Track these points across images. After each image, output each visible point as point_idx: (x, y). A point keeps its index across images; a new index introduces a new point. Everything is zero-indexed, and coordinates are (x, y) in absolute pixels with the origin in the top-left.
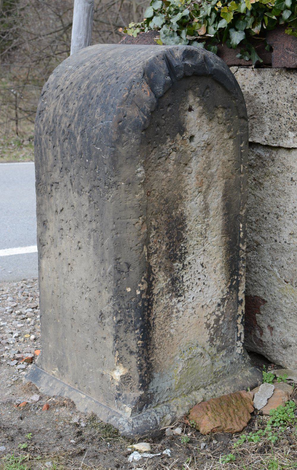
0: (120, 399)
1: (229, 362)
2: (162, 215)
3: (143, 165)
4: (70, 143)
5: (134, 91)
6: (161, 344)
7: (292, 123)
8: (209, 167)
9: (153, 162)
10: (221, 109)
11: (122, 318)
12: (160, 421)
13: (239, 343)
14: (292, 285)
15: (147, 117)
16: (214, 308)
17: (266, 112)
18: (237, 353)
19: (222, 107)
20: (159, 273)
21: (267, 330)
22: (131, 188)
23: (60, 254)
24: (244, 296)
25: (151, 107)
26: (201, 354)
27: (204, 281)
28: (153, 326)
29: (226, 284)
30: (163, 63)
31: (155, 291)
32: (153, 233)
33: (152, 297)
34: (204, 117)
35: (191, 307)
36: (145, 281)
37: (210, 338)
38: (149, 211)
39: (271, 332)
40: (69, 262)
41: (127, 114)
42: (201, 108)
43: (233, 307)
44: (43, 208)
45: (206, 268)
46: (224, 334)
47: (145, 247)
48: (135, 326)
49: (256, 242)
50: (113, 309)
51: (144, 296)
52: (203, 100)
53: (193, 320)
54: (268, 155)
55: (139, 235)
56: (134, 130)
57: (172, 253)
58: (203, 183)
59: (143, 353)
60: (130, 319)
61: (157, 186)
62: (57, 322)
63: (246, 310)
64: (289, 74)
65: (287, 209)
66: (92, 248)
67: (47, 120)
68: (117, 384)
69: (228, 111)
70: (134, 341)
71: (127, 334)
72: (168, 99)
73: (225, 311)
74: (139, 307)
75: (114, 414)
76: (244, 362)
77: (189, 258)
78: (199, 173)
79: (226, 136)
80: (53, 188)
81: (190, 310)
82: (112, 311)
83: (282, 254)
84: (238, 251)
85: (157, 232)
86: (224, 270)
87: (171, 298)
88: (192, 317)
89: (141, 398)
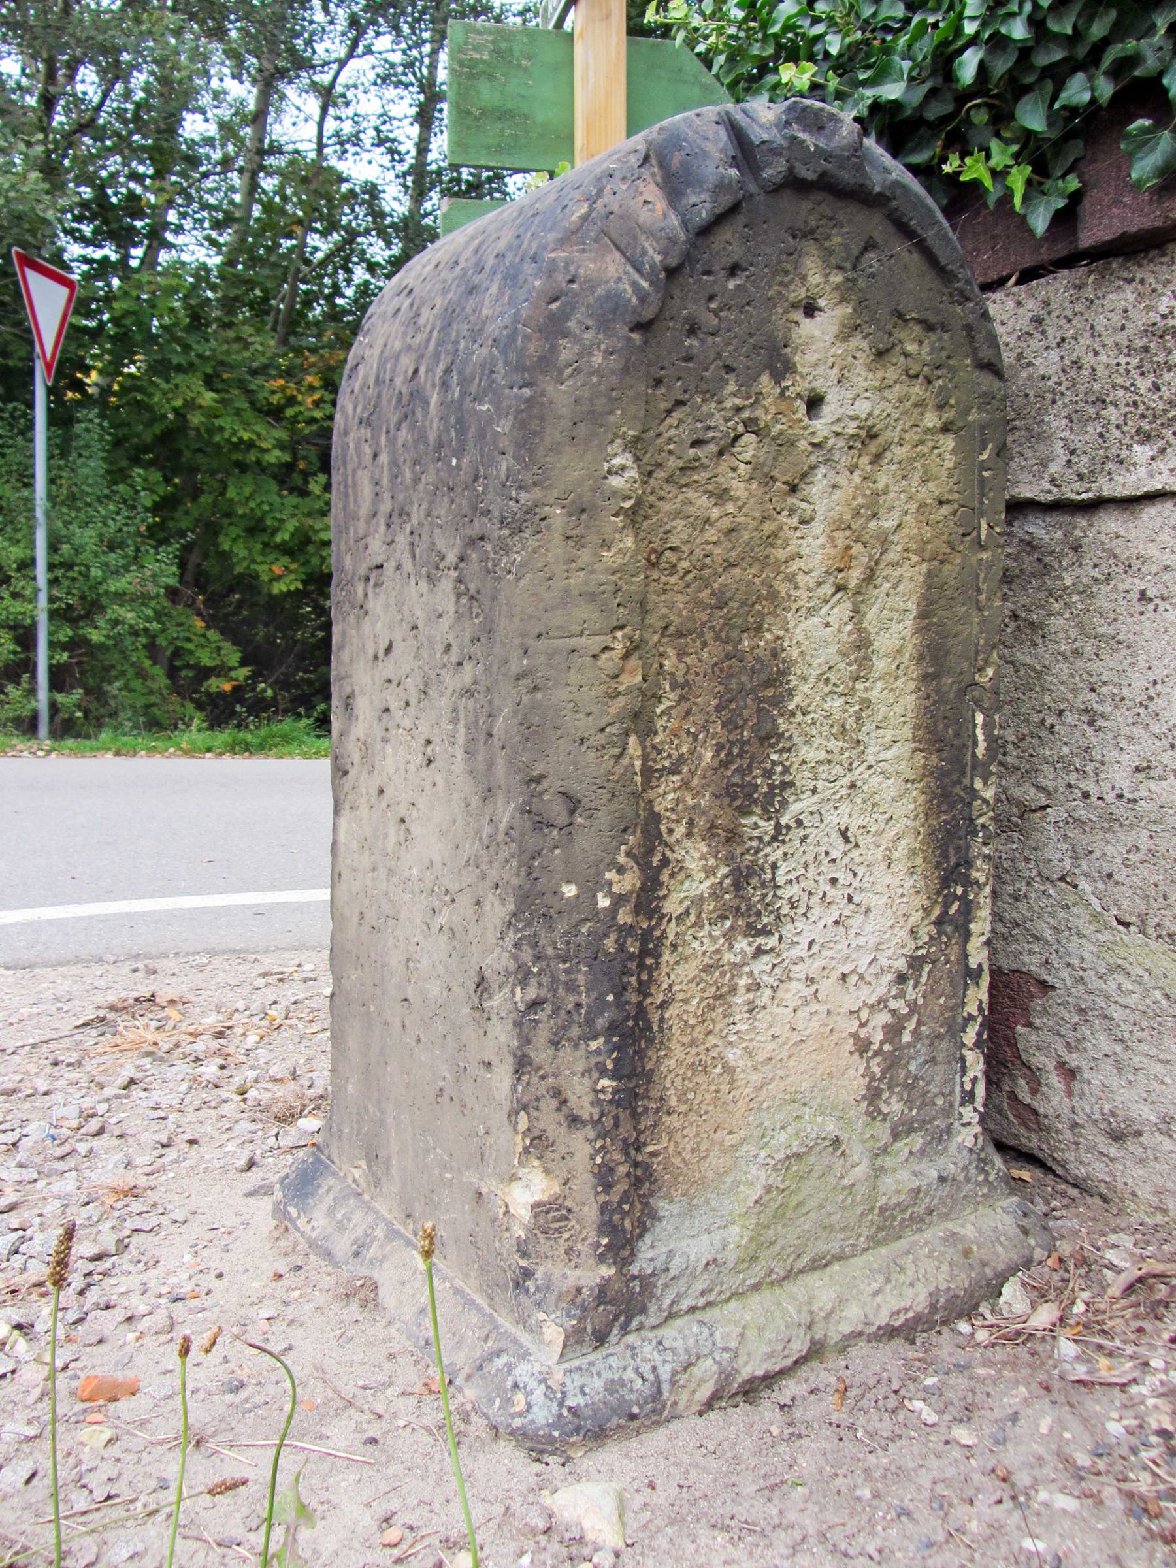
0: (527, 1291)
1: (935, 1174)
2: (704, 644)
3: (635, 446)
4: (412, 428)
6: (691, 1096)
7: (1143, 416)
9: (670, 452)
10: (917, 329)
11: (544, 992)
12: (673, 1383)
13: (969, 1114)
14: (1143, 932)
15: (652, 284)
16: (883, 985)
17: (1054, 402)
18: (960, 1148)
19: (919, 321)
20: (687, 843)
21: (1055, 1079)
22: (587, 527)
24: (985, 952)
25: (664, 253)
26: (836, 1142)
27: (850, 891)
28: (661, 1030)
29: (927, 911)
31: (671, 907)
32: (669, 699)
33: (658, 924)
34: (857, 341)
35: (802, 976)
36: (632, 863)
37: (869, 1087)
38: (652, 620)
39: (1068, 1086)
41: (582, 271)
42: (849, 310)
43: (948, 988)
45: (857, 845)
46: (916, 1078)
47: (633, 740)
48: (589, 1022)
49: (1019, 804)
50: (515, 957)
51: (624, 917)
52: (854, 281)
53: (809, 1024)
54: (1059, 535)
56: (604, 325)
57: (737, 780)
58: (851, 558)
59: (616, 1125)
60: (572, 999)
61: (684, 536)
62: (368, 1013)
63: (991, 1004)
64: (1134, 268)
65: (1126, 692)
66: (460, 754)
68: (521, 1233)
69: (940, 339)
70: (586, 1080)
71: (561, 1053)
73: (920, 1001)
74: (607, 954)
75: (503, 1344)
76: (986, 1179)
78: (840, 525)
79: (931, 420)
81: (795, 990)
82: (512, 966)
83: (1109, 836)
84: (970, 804)
85: (682, 698)
86: (919, 861)
87: (729, 936)
88: (804, 1012)
89: (602, 1294)
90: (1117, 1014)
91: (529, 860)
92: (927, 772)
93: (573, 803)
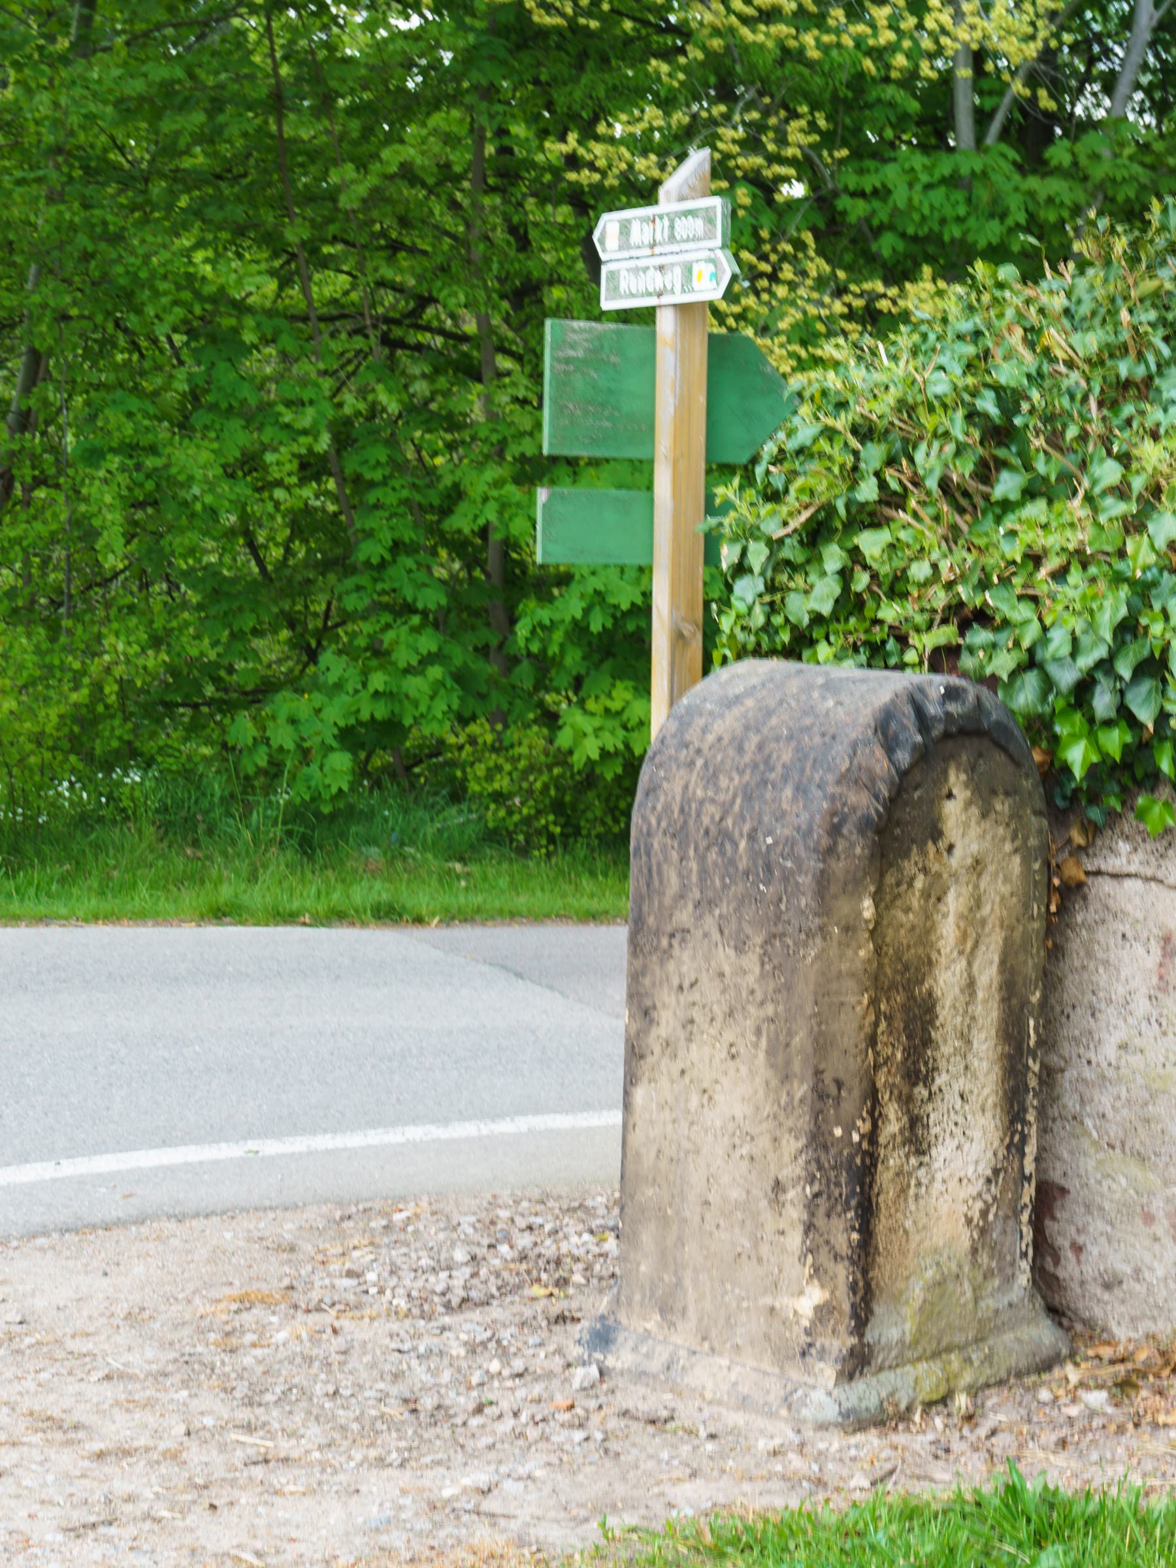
4: (722, 853)
5: (861, 758)
8: (978, 903)
21: (1070, 1255)
23: (683, 1072)
30: (908, 710)
31: (882, 1140)
32: (883, 1025)
40: (705, 1085)
44: (647, 981)
48: (847, 1202)
55: (861, 1028)
56: (862, 831)
66: (762, 1055)
67: (667, 808)
72: (917, 776)
77: (940, 1080)
80: (675, 942)
87: (907, 1156)
89: (852, 1352)
90: (1107, 1205)
91: (817, 1114)
92: (1003, 1056)
93: (839, 1084)
